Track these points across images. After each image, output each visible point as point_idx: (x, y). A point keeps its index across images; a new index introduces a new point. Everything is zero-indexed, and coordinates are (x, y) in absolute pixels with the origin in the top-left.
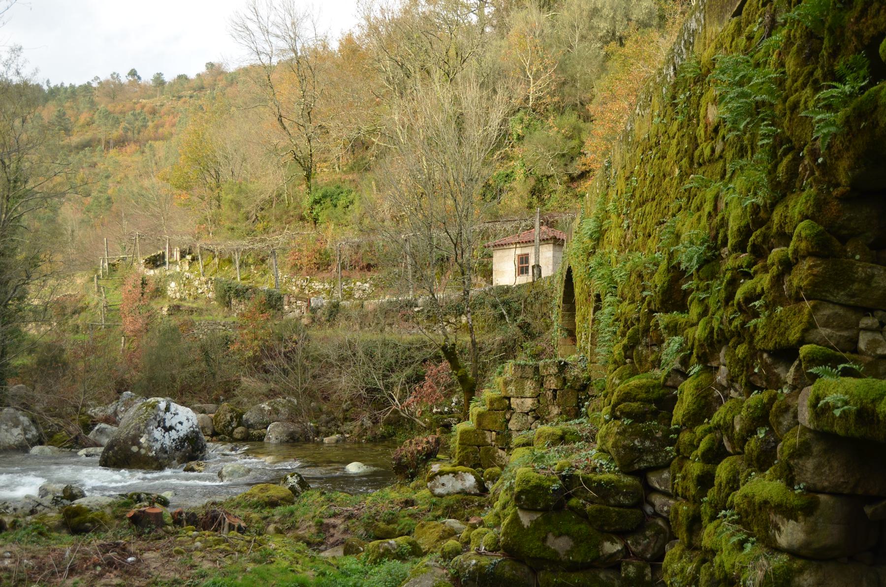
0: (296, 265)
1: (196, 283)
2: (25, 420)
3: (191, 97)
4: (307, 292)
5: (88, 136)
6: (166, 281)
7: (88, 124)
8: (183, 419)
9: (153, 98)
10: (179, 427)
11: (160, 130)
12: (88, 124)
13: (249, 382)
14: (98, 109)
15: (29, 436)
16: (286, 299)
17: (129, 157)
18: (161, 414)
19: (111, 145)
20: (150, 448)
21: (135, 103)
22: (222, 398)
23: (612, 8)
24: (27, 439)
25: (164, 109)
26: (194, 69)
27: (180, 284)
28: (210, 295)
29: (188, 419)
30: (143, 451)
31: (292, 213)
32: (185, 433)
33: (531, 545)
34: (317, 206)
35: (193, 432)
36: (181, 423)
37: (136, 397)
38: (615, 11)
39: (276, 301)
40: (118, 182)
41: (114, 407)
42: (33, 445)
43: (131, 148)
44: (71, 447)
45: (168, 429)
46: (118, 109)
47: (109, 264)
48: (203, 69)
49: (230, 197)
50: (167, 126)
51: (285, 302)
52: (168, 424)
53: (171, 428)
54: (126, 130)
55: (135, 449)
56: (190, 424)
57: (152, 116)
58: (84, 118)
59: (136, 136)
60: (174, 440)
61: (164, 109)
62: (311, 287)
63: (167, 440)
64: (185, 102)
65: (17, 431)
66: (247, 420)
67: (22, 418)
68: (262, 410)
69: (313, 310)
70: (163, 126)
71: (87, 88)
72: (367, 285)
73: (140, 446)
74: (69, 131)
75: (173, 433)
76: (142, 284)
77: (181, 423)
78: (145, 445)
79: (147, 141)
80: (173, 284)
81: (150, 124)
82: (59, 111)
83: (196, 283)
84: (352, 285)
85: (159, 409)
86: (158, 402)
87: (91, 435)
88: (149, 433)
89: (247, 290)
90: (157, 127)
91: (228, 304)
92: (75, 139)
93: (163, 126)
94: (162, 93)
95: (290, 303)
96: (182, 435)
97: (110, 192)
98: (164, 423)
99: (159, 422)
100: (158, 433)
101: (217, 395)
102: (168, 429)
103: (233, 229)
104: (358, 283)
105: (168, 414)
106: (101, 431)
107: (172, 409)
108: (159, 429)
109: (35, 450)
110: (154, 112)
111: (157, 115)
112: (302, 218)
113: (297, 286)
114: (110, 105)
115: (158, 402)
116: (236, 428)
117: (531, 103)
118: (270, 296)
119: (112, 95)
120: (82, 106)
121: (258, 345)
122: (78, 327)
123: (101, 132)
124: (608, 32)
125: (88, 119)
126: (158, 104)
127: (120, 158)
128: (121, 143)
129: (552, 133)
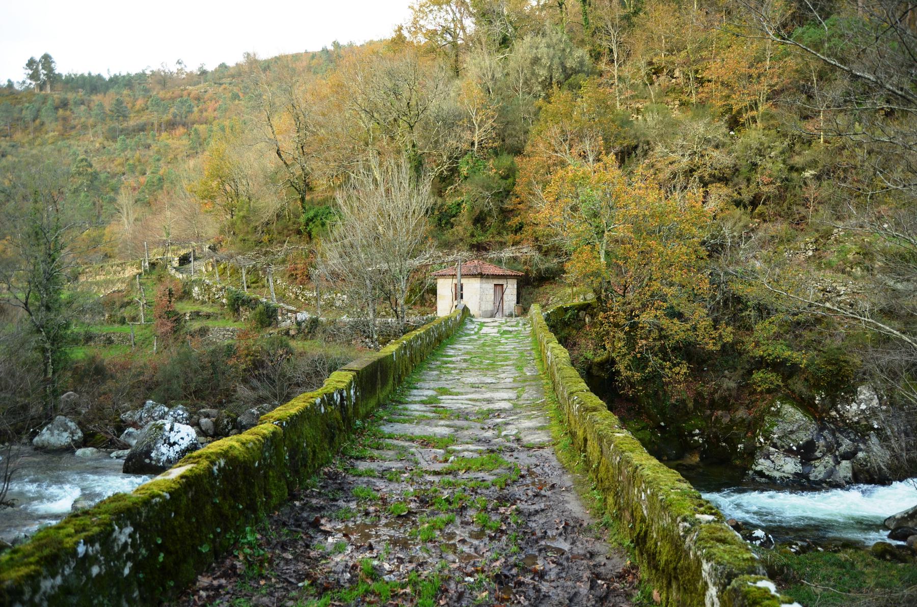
0: (292, 275)
1: (214, 289)
2: (72, 425)
3: (230, 84)
4: (300, 298)
5: (144, 119)
6: (192, 285)
7: (143, 110)
8: (184, 436)
9: (198, 84)
10: (181, 442)
11: (205, 114)
12: (143, 110)
13: (243, 391)
14: (151, 96)
15: (76, 438)
16: (279, 311)
17: (178, 141)
18: (167, 434)
19: (163, 128)
20: (158, 460)
21: (182, 90)
22: (224, 401)
23: (549, 58)
24: (73, 440)
25: (207, 96)
26: (234, 59)
27: (202, 289)
28: (224, 301)
29: (188, 435)
30: (154, 463)
31: (291, 228)
32: (186, 446)
33: (706, 281)
34: (311, 223)
35: (192, 444)
36: (182, 438)
37: (157, 405)
38: (552, 60)
39: (272, 312)
40: (169, 163)
41: (139, 413)
42: (79, 447)
43: (181, 130)
44: (106, 447)
45: (172, 445)
46: (168, 96)
47: (149, 263)
48: (241, 59)
49: (241, 214)
50: (210, 110)
51: (279, 314)
52: (172, 441)
53: (175, 443)
54: (175, 116)
55: (147, 461)
56: (190, 438)
57: (196, 102)
58: (140, 103)
59: (184, 119)
60: (177, 452)
61: (207, 96)
62: (303, 295)
63: (172, 453)
64: (225, 89)
65: (66, 435)
66: (241, 422)
67: (70, 424)
68: (253, 414)
69: (299, 324)
70: (206, 111)
71: (142, 77)
72: (345, 296)
73: (151, 459)
74: (126, 117)
75: (177, 448)
76: (169, 294)
77: (182, 438)
78: (155, 458)
79: (193, 124)
80: (196, 289)
81: (196, 109)
82: (117, 100)
83: (214, 289)
84: (334, 296)
85: (165, 430)
86: (164, 424)
87: (122, 437)
88: (157, 450)
89: (251, 300)
90: (201, 111)
91: (237, 310)
92: (132, 123)
93: (206, 111)
94: (206, 81)
95: (283, 314)
96: (183, 448)
97: (161, 172)
98: (169, 440)
99: (165, 440)
100: (164, 449)
101: (220, 399)
102: (172, 445)
103: (244, 240)
104: (339, 295)
105: (173, 433)
106: (129, 434)
107: (176, 429)
108: (165, 445)
109: (79, 452)
110: (198, 99)
111: (202, 101)
112: (299, 232)
113: (293, 293)
114: (161, 92)
115: (164, 424)
116: (232, 430)
117: (476, 147)
118: (267, 308)
119: (163, 82)
120: (137, 93)
121: (250, 360)
122: (125, 319)
123: (153, 117)
124: (546, 78)
125: (143, 105)
126: (203, 90)
127: (170, 142)
128: (171, 125)
129: (492, 173)
